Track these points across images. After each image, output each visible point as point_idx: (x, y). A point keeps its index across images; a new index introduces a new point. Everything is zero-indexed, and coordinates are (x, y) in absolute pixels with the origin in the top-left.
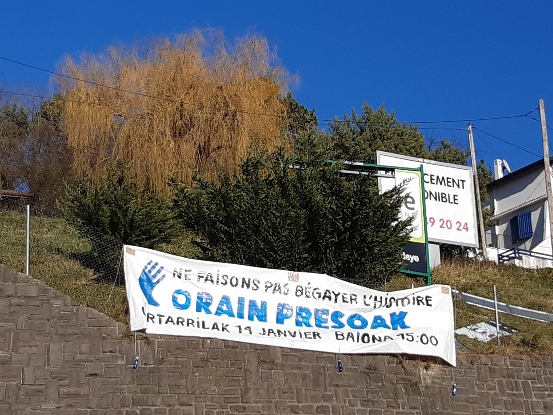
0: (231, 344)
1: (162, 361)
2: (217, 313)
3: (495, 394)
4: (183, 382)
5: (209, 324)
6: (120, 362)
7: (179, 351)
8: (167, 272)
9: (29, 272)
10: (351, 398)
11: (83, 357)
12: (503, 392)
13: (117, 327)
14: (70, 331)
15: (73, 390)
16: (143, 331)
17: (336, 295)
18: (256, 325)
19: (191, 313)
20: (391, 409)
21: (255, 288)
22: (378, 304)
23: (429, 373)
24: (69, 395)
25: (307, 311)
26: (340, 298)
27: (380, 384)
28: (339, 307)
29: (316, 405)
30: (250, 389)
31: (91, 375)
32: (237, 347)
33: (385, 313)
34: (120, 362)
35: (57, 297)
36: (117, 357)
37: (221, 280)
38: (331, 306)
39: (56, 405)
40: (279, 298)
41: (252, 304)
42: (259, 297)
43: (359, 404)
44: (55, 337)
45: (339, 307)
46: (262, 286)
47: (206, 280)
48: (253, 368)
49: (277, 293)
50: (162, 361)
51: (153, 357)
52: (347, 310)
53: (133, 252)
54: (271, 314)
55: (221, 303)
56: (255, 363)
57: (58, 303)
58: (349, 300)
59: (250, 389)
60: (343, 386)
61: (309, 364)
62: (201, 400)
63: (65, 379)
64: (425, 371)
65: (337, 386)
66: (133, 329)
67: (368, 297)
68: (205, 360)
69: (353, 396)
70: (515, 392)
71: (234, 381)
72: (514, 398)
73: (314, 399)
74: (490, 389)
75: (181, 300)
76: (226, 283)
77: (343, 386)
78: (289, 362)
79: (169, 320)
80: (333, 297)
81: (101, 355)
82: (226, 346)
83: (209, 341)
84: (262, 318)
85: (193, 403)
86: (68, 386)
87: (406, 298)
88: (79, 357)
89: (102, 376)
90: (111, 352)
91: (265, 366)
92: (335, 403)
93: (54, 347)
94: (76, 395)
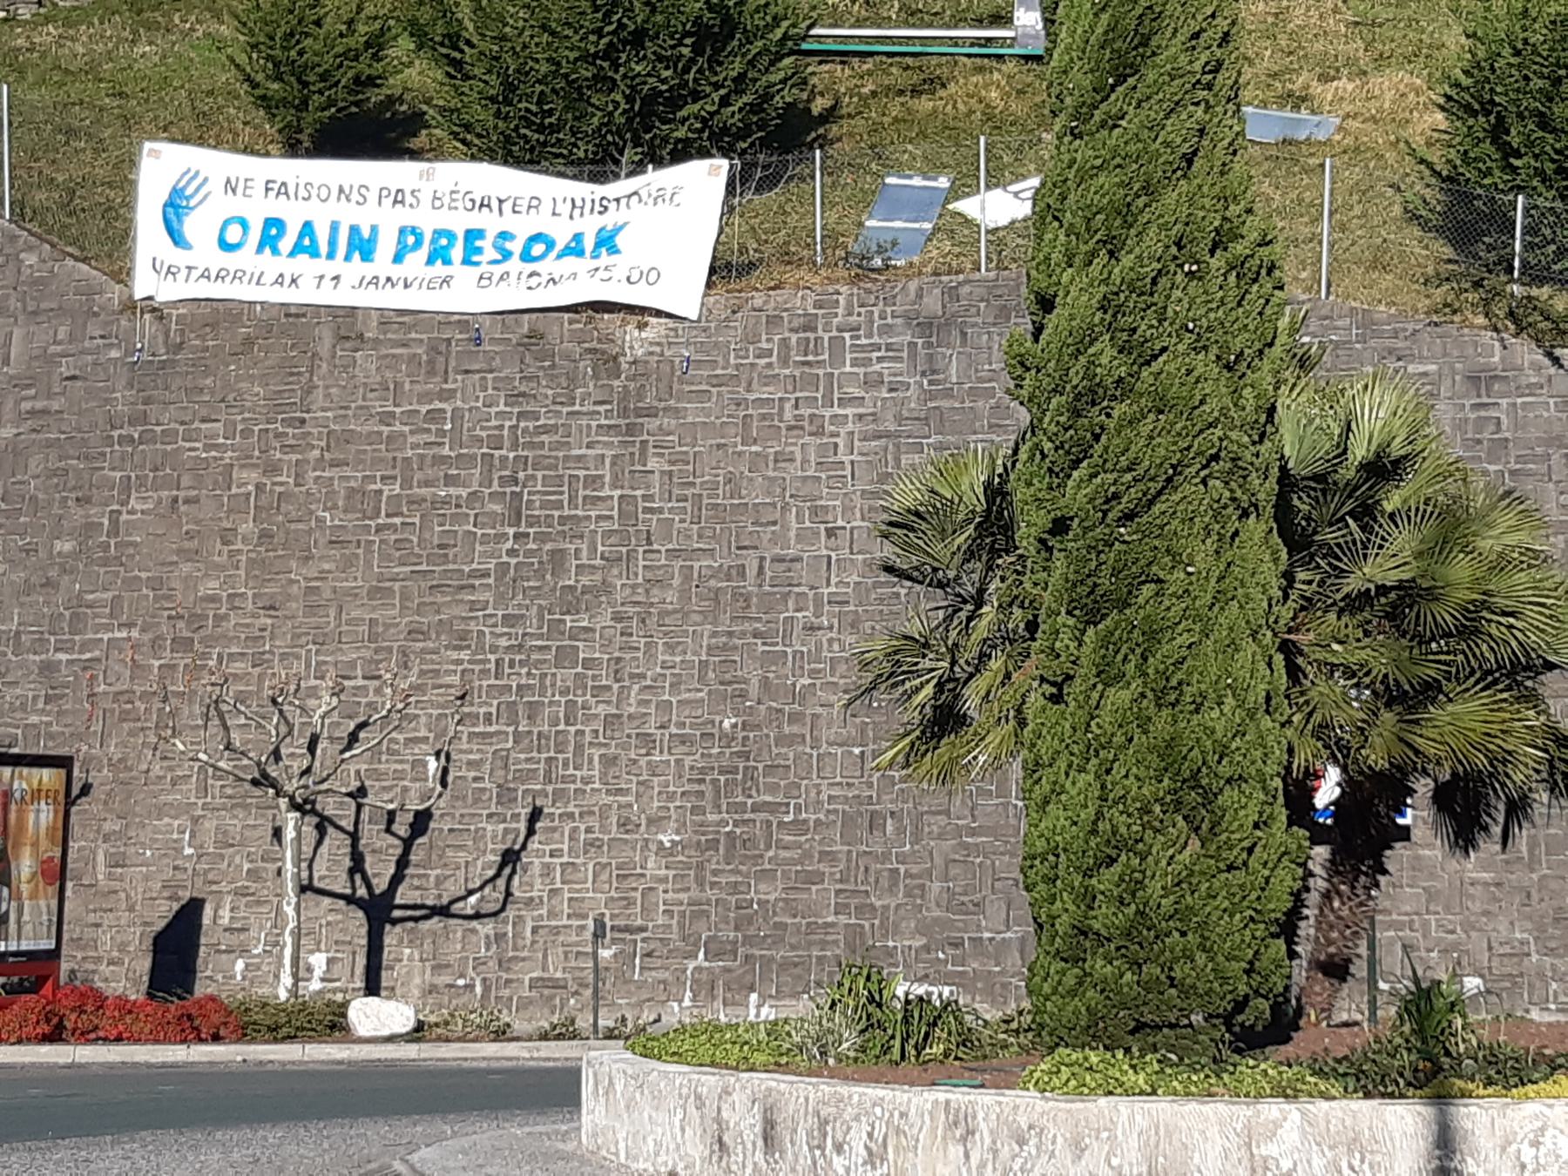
0: (293, 310)
1: (180, 347)
2: (292, 254)
3: (770, 365)
4: (208, 381)
5: (269, 278)
6: (114, 354)
7: (208, 329)
8: (216, 185)
9: (12, 210)
10: (490, 391)
11: (59, 348)
12: (784, 361)
13: (115, 292)
14: (44, 306)
15: (39, 405)
16: (150, 298)
17: (501, 201)
18: (356, 269)
19: (246, 258)
20: (559, 408)
21: (361, 200)
22: (577, 212)
23: (644, 335)
24: (33, 413)
25: (451, 235)
26: (507, 206)
27: (547, 364)
28: (509, 222)
29: (424, 409)
30: (317, 387)
31: (67, 379)
32: (304, 315)
33: (590, 226)
34: (114, 354)
35: (30, 249)
36: (111, 345)
37: (302, 193)
38: (460, 222)
39: (15, 431)
40: (404, 216)
41: (354, 230)
42: (364, 217)
43: (502, 401)
44: (21, 318)
45: (509, 222)
46: (373, 196)
47: (279, 193)
48: (324, 349)
49: (399, 206)
50: (180, 347)
51: (166, 343)
52: (523, 227)
53: (155, 154)
54: (386, 246)
55: (301, 236)
56: (328, 340)
57: (30, 259)
58: (524, 209)
59: (317, 387)
60: (478, 371)
61: (424, 336)
62: (234, 410)
63: (29, 386)
64: (636, 333)
65: (467, 372)
66: (137, 296)
67: (560, 202)
68: (249, 342)
69: (494, 389)
70: (810, 358)
71: (292, 374)
72: (807, 370)
73: (424, 397)
74: (759, 357)
75: (233, 234)
76: (309, 198)
77: (478, 371)
78: (389, 336)
79: (205, 275)
80: (495, 204)
81: (87, 344)
82: (287, 315)
83: (258, 308)
84: (367, 256)
85: (223, 417)
86: (34, 398)
87: (635, 193)
88: (53, 349)
89: (86, 379)
90: (102, 337)
91: (348, 345)
92: (459, 403)
93: (17, 334)
94: (45, 412)
